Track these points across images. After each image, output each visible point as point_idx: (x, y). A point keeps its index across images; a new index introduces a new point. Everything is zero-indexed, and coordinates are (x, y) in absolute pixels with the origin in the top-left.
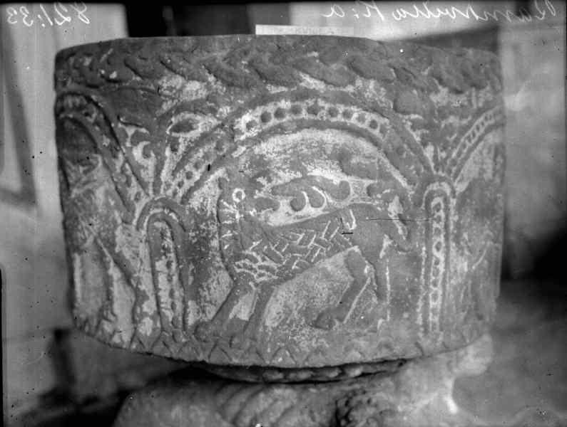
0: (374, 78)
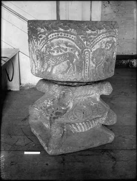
0: (73, 28)
